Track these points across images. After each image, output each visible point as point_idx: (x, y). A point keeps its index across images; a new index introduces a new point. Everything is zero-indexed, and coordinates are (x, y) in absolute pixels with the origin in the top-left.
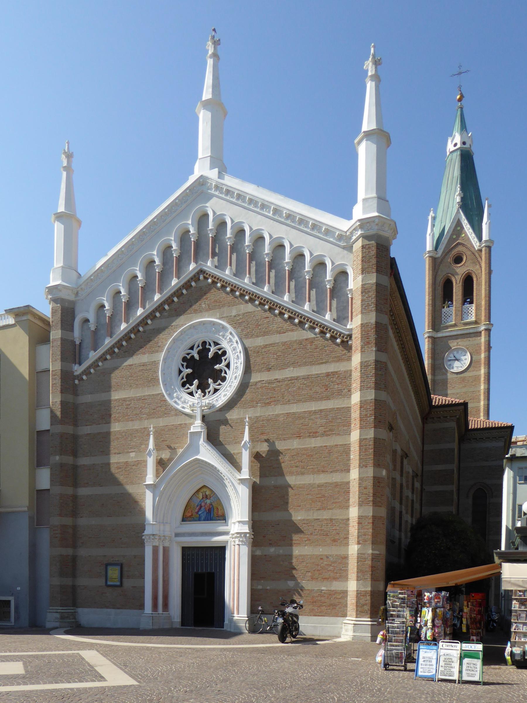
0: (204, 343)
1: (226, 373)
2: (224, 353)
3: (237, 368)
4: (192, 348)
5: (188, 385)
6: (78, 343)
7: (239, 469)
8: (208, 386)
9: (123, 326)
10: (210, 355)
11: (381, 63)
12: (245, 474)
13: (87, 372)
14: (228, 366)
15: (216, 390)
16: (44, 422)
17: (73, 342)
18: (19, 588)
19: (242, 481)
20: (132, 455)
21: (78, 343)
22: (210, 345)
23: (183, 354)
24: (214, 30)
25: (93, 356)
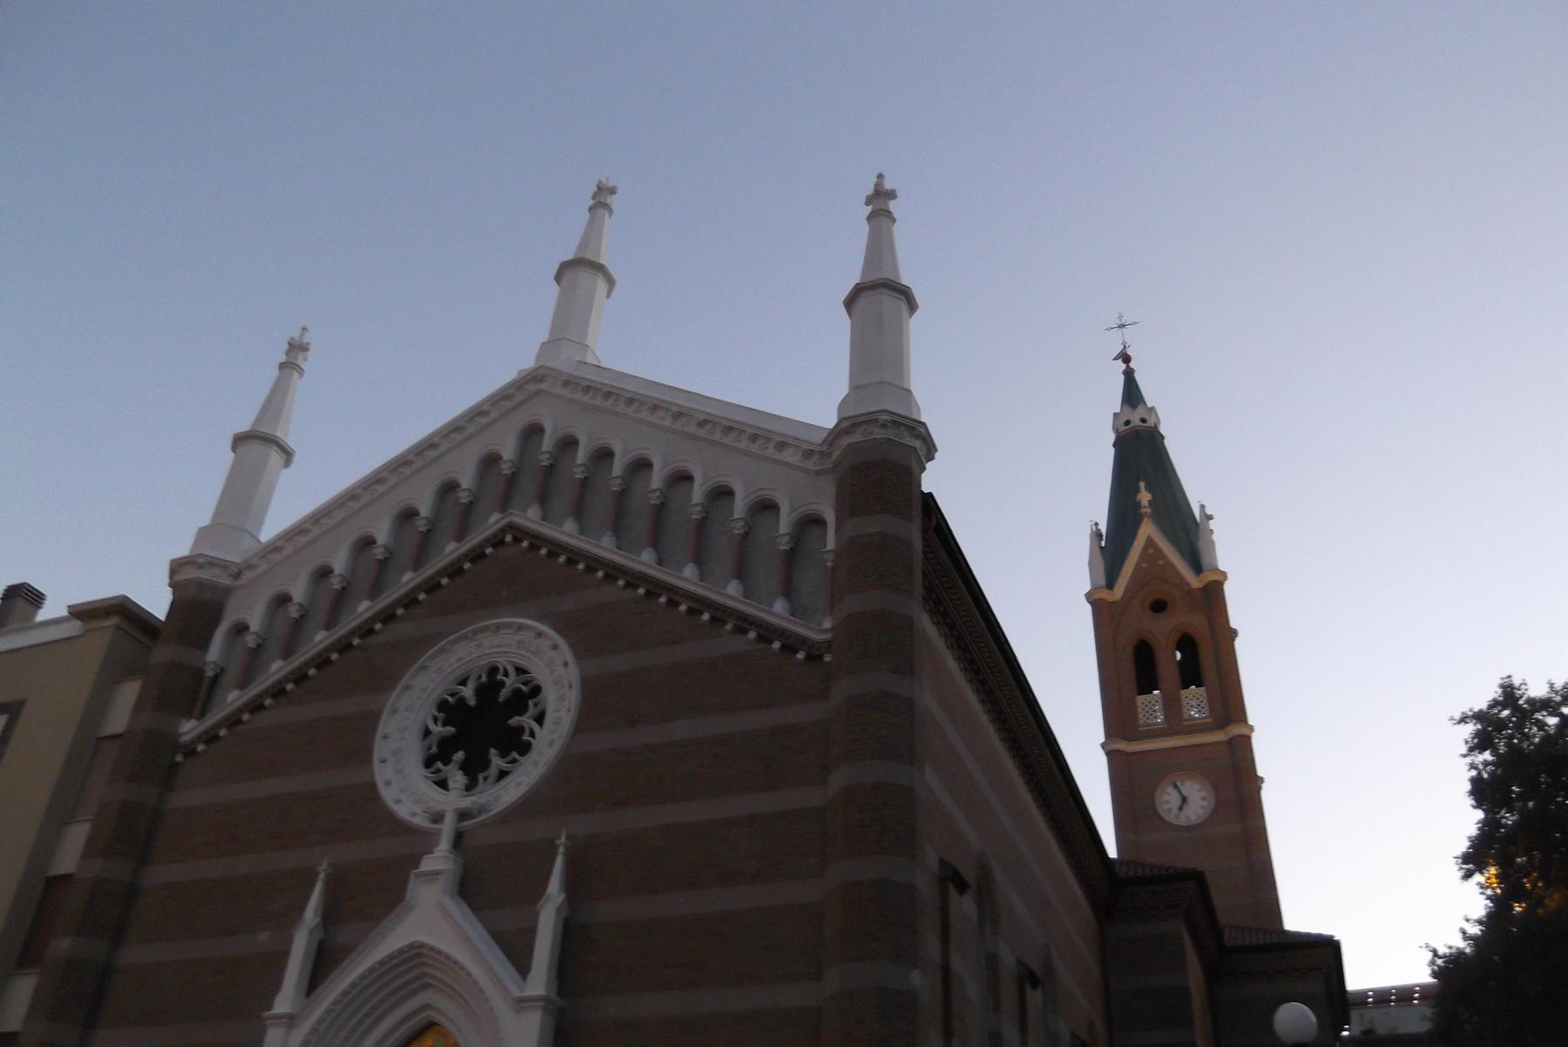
0: (493, 670)
1: (532, 735)
2: (536, 690)
3: (557, 723)
4: (463, 682)
5: (439, 765)
6: (210, 673)
7: (523, 968)
8: (486, 764)
9: (276, 665)
10: (504, 694)
11: (869, 201)
12: (539, 982)
13: (210, 738)
14: (540, 719)
15: (503, 774)
16: (67, 859)
17: (200, 673)
18: (1179, 656)
19: (521, 1004)
20: (263, 936)
21: (210, 673)
22: (506, 674)
23: (502, 662)
24: (304, 329)
25: (233, 698)
